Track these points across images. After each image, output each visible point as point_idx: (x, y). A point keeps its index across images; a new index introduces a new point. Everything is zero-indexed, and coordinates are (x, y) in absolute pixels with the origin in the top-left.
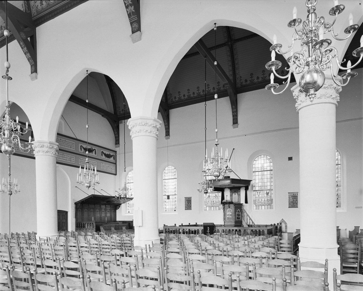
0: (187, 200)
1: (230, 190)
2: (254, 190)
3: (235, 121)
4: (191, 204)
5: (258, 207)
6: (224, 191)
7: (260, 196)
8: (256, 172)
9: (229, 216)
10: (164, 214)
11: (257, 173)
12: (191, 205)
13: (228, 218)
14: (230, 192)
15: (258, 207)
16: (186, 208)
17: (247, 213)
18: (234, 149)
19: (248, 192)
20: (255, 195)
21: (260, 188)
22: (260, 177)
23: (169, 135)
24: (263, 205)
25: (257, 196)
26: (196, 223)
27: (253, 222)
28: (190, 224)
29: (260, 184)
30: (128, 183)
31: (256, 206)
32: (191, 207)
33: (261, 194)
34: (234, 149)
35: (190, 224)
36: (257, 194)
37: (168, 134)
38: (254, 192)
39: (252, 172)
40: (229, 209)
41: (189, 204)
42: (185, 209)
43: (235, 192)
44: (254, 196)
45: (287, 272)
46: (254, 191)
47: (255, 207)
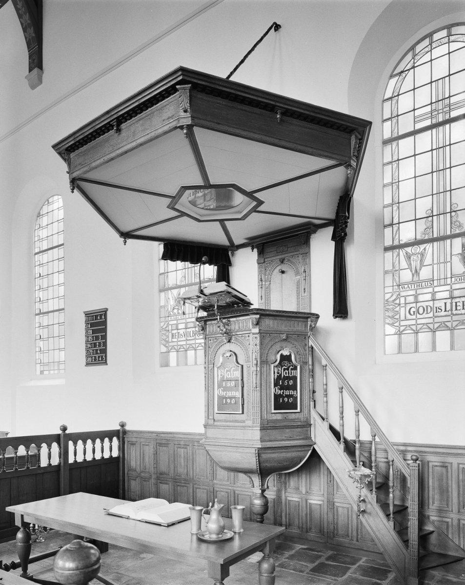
0: (92, 325)
1: (261, 253)
2: (388, 242)
4: (104, 337)
5: (408, 339)
6: (229, 263)
7: (425, 273)
8: (401, 142)
9: (226, 389)
10: (32, 383)
11: (405, 146)
12: (105, 344)
13: (221, 398)
14: (256, 265)
15: (408, 339)
16: (90, 359)
17: (340, 374)
18: (277, 27)
19: (352, 254)
20: (395, 271)
21: (422, 225)
22: (424, 163)
23: (40, 66)
24: (444, 326)
25: (406, 276)
26: (64, 429)
27: (376, 431)
28: (67, 432)
29: (424, 206)
30: (40, 313)
31: (400, 334)
32: (104, 351)
33: (428, 260)
34: (277, 27)
35: (67, 432)
36: (404, 264)
37: (36, 61)
38: (389, 254)
39: (380, 143)
40: (228, 346)
41: (97, 338)
42: (88, 364)
44: (389, 278)
45: (294, 299)
46: (387, 249)
47: (391, 342)
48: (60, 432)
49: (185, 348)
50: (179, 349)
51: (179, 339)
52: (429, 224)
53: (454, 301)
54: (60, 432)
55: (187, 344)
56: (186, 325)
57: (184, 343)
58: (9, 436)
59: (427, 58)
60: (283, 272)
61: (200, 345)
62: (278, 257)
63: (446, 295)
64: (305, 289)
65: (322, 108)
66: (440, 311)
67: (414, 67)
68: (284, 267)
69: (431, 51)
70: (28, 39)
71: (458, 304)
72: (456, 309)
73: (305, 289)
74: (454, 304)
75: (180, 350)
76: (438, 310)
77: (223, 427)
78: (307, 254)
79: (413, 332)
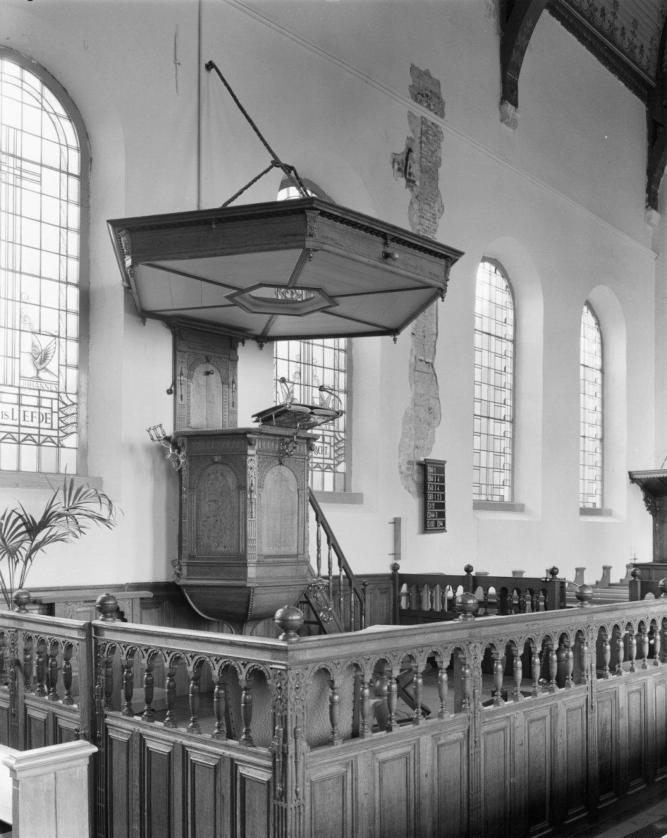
3: (509, 93)
26: (468, 569)
35: (400, 571)
43: (208, 361)
48: (465, 573)
49: (37, 440)
50: (44, 442)
51: (23, 423)
52: (298, 370)
53: (23, 408)
54: (465, 573)
55: (323, 464)
56: (39, 402)
57: (321, 461)
58: (488, 575)
59: (493, 284)
60: (208, 373)
61: (29, 438)
62: (204, 352)
63: (34, 401)
64: (182, 396)
65: (259, 204)
66: (6, 417)
67: (43, 109)
68: (210, 368)
69: (21, 88)
70: (514, 94)
71: (26, 413)
72: (24, 420)
73: (182, 396)
74: (22, 413)
75: (24, 442)
76: (4, 416)
77: (290, 564)
78: (235, 361)
79: (54, 445)
